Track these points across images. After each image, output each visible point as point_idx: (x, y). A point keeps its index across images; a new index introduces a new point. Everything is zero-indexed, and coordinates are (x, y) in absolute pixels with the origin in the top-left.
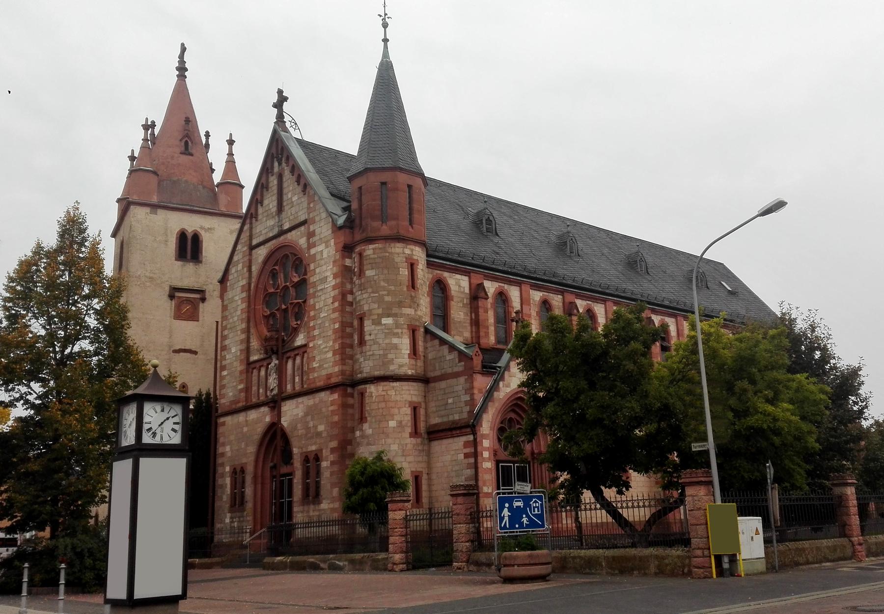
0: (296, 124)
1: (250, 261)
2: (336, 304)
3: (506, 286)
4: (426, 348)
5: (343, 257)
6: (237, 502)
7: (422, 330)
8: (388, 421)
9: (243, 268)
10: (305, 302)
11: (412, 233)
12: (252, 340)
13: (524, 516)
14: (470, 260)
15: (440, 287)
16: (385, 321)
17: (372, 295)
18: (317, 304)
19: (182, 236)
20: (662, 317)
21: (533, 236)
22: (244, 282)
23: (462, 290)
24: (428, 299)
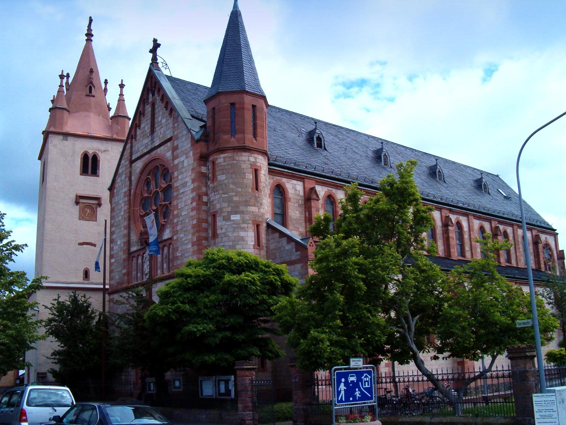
0: (166, 64)
2: (194, 204)
3: (334, 191)
4: (268, 240)
7: (265, 225)
9: (125, 178)
10: (170, 203)
11: (253, 144)
12: (131, 235)
13: (357, 390)
14: (303, 168)
15: (279, 190)
16: (233, 217)
17: (223, 196)
18: (180, 205)
19: (85, 157)
20: (457, 216)
21: (354, 152)
22: (126, 189)
23: (298, 193)
24: (269, 200)
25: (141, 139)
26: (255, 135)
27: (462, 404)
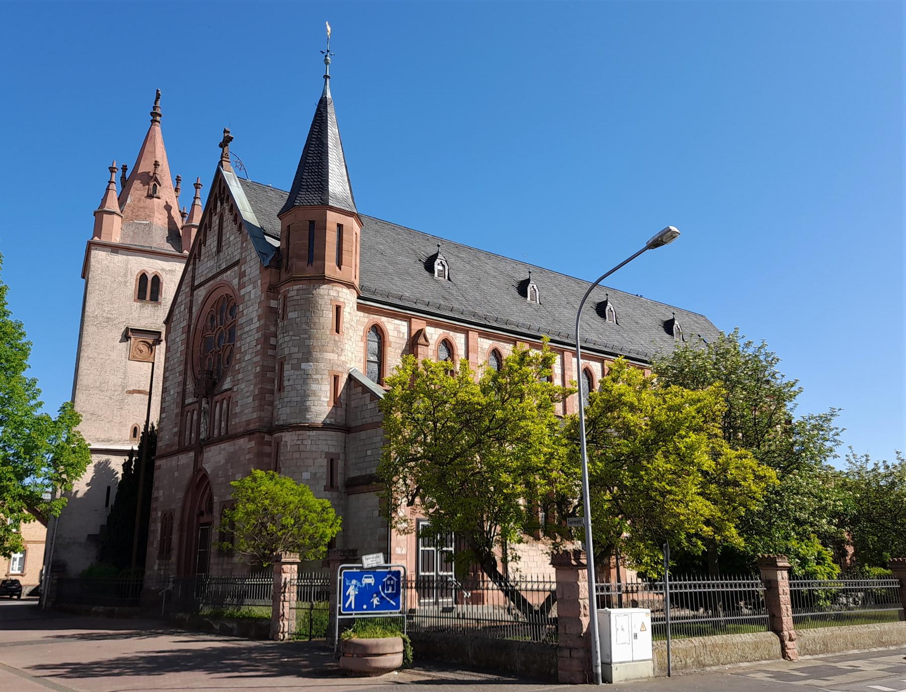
1: (191, 301)
3: (451, 333)
5: (268, 298)
6: (165, 550)
7: (346, 376)
8: (302, 472)
9: (185, 310)
17: (293, 338)
19: (143, 277)
22: (185, 323)
23: (401, 335)
25: (206, 259)
26: (339, 264)
27: (484, 618)
